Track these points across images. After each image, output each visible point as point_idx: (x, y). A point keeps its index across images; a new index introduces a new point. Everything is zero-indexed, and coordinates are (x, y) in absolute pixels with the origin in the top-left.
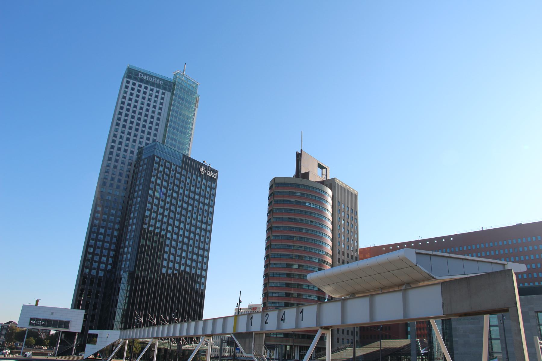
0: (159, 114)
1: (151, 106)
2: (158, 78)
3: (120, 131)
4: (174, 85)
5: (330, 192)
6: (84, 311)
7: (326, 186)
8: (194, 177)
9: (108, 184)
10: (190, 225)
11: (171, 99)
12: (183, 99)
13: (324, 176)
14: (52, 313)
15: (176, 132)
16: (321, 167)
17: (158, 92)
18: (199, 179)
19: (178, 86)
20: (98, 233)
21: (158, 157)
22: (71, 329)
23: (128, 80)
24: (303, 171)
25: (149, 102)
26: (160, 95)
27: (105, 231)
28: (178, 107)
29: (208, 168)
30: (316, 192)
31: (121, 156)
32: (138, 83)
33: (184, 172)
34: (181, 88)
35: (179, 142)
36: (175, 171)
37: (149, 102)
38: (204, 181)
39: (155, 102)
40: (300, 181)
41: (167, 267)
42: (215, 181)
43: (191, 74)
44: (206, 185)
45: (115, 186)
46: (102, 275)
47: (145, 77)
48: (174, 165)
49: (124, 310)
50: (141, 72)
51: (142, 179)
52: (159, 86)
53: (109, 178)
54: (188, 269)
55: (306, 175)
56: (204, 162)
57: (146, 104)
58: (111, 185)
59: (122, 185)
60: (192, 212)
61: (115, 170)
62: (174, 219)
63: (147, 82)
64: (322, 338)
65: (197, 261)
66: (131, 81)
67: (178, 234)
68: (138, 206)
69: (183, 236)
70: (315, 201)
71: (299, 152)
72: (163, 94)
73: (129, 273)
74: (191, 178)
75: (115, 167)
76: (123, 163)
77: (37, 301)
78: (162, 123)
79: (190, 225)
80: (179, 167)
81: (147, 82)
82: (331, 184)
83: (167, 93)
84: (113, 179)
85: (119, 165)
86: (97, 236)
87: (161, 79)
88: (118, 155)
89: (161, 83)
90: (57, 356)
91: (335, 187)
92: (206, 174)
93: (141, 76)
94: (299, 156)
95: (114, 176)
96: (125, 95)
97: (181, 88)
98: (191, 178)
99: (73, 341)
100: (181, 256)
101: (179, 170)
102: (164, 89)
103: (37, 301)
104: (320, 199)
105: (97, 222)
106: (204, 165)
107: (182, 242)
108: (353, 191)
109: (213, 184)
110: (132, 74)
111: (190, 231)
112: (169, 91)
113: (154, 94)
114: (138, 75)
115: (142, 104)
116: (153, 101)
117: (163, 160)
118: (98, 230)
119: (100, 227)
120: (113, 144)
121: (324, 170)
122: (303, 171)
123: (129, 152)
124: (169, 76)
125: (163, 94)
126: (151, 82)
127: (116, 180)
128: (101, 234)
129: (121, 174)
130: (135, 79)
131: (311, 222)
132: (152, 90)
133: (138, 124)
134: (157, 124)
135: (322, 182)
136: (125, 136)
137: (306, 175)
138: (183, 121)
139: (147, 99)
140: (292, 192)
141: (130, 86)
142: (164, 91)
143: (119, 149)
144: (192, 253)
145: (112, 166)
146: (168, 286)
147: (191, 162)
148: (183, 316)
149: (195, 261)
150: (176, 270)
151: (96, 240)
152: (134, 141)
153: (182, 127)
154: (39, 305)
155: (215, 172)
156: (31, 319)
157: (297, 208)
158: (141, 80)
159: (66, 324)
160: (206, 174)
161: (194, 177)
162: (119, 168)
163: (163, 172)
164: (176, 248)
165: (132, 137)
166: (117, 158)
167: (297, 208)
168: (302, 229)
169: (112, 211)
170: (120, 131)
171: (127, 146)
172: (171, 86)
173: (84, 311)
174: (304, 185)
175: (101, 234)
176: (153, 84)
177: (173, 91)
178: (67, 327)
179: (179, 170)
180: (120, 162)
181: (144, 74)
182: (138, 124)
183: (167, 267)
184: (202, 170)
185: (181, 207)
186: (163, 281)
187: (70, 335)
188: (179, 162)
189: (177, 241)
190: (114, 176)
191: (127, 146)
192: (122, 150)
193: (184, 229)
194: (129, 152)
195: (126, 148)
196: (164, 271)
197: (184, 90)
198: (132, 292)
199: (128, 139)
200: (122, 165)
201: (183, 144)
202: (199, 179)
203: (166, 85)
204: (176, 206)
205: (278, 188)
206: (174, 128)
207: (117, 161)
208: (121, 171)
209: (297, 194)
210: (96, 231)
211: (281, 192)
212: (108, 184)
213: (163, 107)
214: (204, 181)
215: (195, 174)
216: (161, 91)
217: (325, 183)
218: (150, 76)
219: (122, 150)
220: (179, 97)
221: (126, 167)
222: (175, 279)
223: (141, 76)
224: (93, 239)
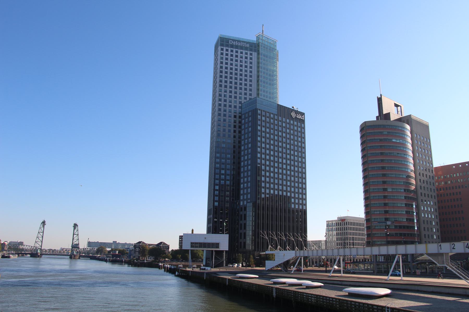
0: (251, 72)
1: (244, 66)
2: (244, 42)
3: (223, 91)
4: (259, 46)
5: (408, 127)
6: (228, 235)
7: (404, 122)
8: (288, 121)
9: (221, 135)
10: (290, 159)
11: (258, 58)
12: (267, 57)
13: (400, 112)
14: (205, 238)
15: (266, 85)
16: (396, 106)
17: (246, 54)
18: (292, 122)
19: (261, 46)
20: (220, 174)
21: (260, 110)
22: (221, 248)
23: (222, 47)
24: (385, 112)
25: (241, 64)
26: (249, 56)
27: (225, 172)
28: (264, 64)
29: (297, 112)
30: (399, 130)
31: (227, 111)
32: (230, 49)
33: (280, 118)
34: (264, 47)
35: (270, 93)
36: (274, 118)
37: (241, 64)
38: (295, 123)
39: (246, 62)
40: (384, 122)
41: (265, 193)
42: (303, 121)
43: (271, 34)
44: (297, 126)
45: (227, 136)
46: (228, 206)
47: (234, 43)
48: (272, 114)
49: (252, 231)
50: (230, 39)
51: (250, 129)
52: (246, 49)
53: (222, 131)
54: (276, 192)
55: (388, 115)
56: (293, 107)
57: (239, 66)
58: (224, 136)
59: (232, 134)
60: (290, 149)
61: (225, 123)
62: (278, 157)
63: (237, 47)
64: (301, 259)
65: (298, 188)
66: (225, 48)
67: (282, 169)
68: (250, 150)
69: (286, 169)
70: (399, 137)
71: (379, 96)
72: (251, 54)
73: (253, 204)
74: (286, 122)
75: (225, 120)
76: (230, 117)
77: (193, 230)
78: (254, 79)
79: (290, 159)
80: (276, 115)
81: (237, 47)
82: (408, 120)
83: (253, 53)
84: (224, 130)
85: (227, 118)
86: (220, 177)
87: (247, 43)
88: (225, 111)
89: (248, 45)
90: (215, 267)
91: (411, 122)
92: (296, 117)
93: (231, 42)
94: (380, 100)
95: (225, 128)
96: (221, 60)
97: (264, 47)
98: (286, 122)
99: (222, 257)
100: (286, 185)
101: (276, 117)
102: (251, 50)
103: (193, 230)
104: (401, 134)
105: (218, 166)
106: (294, 110)
107: (286, 175)
108: (425, 123)
109: (302, 125)
110: (224, 42)
111: (290, 165)
112: (255, 51)
113: (244, 56)
114: (228, 42)
115: (236, 66)
116: (244, 62)
117: (264, 111)
118: (220, 171)
119: (220, 169)
120: (220, 102)
121: (399, 108)
122: (385, 112)
123: (233, 106)
124: (253, 39)
125: (251, 54)
126: (240, 46)
127: (227, 131)
128: (223, 174)
129: (230, 126)
130: (227, 46)
131: (398, 154)
132: (242, 53)
133: (236, 83)
134: (251, 81)
135: (400, 120)
136: (228, 94)
137: (388, 115)
138: (270, 75)
139: (239, 61)
140: (381, 132)
141: (225, 52)
142: (251, 52)
143: (225, 106)
144: (294, 182)
145: (222, 120)
146: (281, 209)
147: (284, 109)
148: (293, 231)
149: (268, 183)
150: (268, 194)
151: (220, 179)
152: (236, 97)
153: (270, 80)
154: (194, 233)
155: (303, 114)
156: (192, 243)
157: (384, 142)
158: (232, 46)
159: (217, 245)
160: (296, 117)
161: (288, 121)
162: (227, 121)
163: (265, 121)
164: (282, 179)
165: (233, 95)
166: (225, 113)
167: (384, 142)
168: (392, 160)
169: (228, 156)
170: (223, 91)
171: (230, 102)
172: (256, 47)
173: (228, 235)
174: (389, 125)
175: (223, 174)
176: (242, 48)
177: (258, 51)
178: (218, 247)
179: (276, 117)
180: (227, 116)
181: (234, 40)
182: (236, 83)
183: (265, 193)
184: (293, 114)
185: (282, 147)
186: (276, 206)
187: (220, 253)
188: (275, 111)
189: (282, 174)
190: (225, 128)
191: (230, 102)
192: (228, 106)
193: (286, 164)
194: (233, 106)
195: (230, 104)
196: (263, 196)
197: (267, 48)
198: (257, 217)
199: (230, 97)
200: (230, 118)
201: (273, 94)
202: (292, 122)
203: (252, 46)
204: (278, 146)
205: (367, 130)
206: (264, 82)
207: (225, 115)
208: (230, 123)
209: (385, 133)
210: (218, 172)
211: (371, 133)
212: (221, 135)
213: (253, 65)
214: (295, 123)
215: (288, 119)
216: (249, 52)
217: (402, 120)
218: (239, 41)
219: (228, 106)
220: (264, 56)
221: (233, 119)
222: (272, 202)
223: (231, 42)
224: (217, 179)
